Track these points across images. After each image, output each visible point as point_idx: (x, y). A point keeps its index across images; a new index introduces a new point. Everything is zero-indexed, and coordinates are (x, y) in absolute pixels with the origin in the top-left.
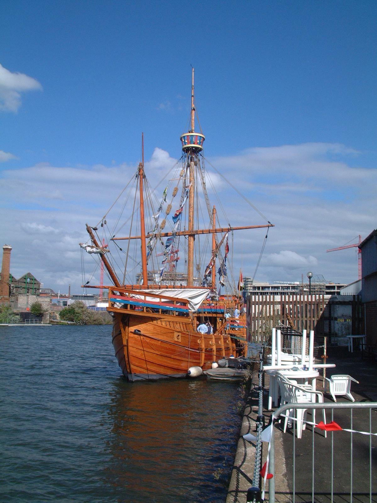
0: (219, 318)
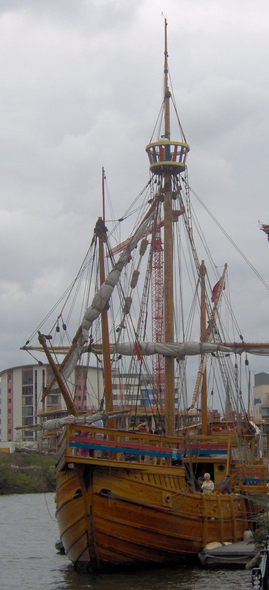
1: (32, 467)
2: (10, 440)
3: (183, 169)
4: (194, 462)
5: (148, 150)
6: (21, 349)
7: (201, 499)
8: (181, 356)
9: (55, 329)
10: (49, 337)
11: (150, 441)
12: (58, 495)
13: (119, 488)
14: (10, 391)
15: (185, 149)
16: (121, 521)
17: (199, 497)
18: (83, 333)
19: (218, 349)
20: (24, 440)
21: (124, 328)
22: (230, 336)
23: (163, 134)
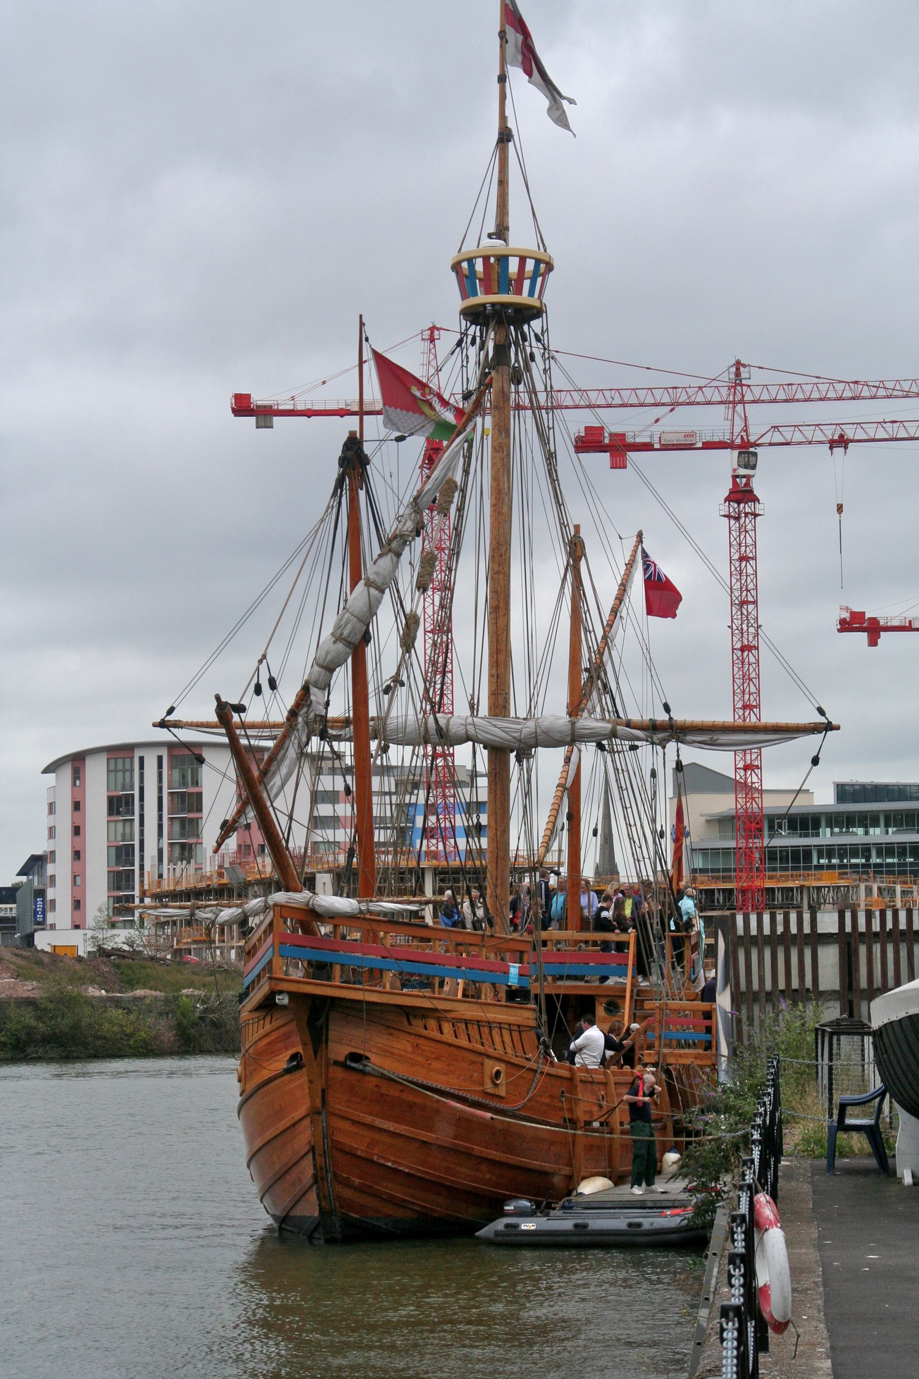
0: (605, 1000)
1: (139, 992)
2: (77, 927)
3: (537, 312)
4: (548, 992)
5: (456, 267)
6: (154, 725)
7: (571, 1079)
8: (524, 752)
9: (252, 688)
10: (240, 709)
11: (457, 945)
12: (245, 1065)
13: (388, 1054)
14: (77, 806)
15: (542, 266)
16: (403, 1129)
17: (565, 1073)
18: (312, 697)
19: (614, 734)
20: (113, 925)
21: (402, 684)
22: (638, 701)
23: (492, 230)
